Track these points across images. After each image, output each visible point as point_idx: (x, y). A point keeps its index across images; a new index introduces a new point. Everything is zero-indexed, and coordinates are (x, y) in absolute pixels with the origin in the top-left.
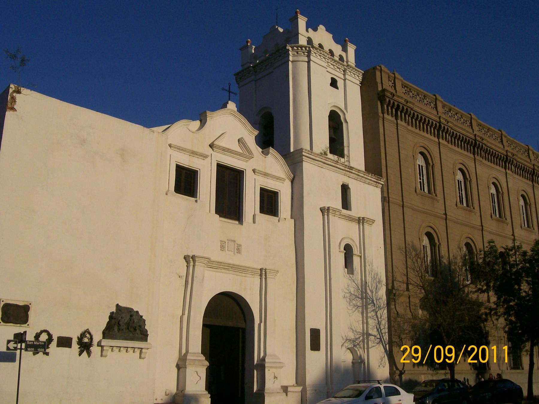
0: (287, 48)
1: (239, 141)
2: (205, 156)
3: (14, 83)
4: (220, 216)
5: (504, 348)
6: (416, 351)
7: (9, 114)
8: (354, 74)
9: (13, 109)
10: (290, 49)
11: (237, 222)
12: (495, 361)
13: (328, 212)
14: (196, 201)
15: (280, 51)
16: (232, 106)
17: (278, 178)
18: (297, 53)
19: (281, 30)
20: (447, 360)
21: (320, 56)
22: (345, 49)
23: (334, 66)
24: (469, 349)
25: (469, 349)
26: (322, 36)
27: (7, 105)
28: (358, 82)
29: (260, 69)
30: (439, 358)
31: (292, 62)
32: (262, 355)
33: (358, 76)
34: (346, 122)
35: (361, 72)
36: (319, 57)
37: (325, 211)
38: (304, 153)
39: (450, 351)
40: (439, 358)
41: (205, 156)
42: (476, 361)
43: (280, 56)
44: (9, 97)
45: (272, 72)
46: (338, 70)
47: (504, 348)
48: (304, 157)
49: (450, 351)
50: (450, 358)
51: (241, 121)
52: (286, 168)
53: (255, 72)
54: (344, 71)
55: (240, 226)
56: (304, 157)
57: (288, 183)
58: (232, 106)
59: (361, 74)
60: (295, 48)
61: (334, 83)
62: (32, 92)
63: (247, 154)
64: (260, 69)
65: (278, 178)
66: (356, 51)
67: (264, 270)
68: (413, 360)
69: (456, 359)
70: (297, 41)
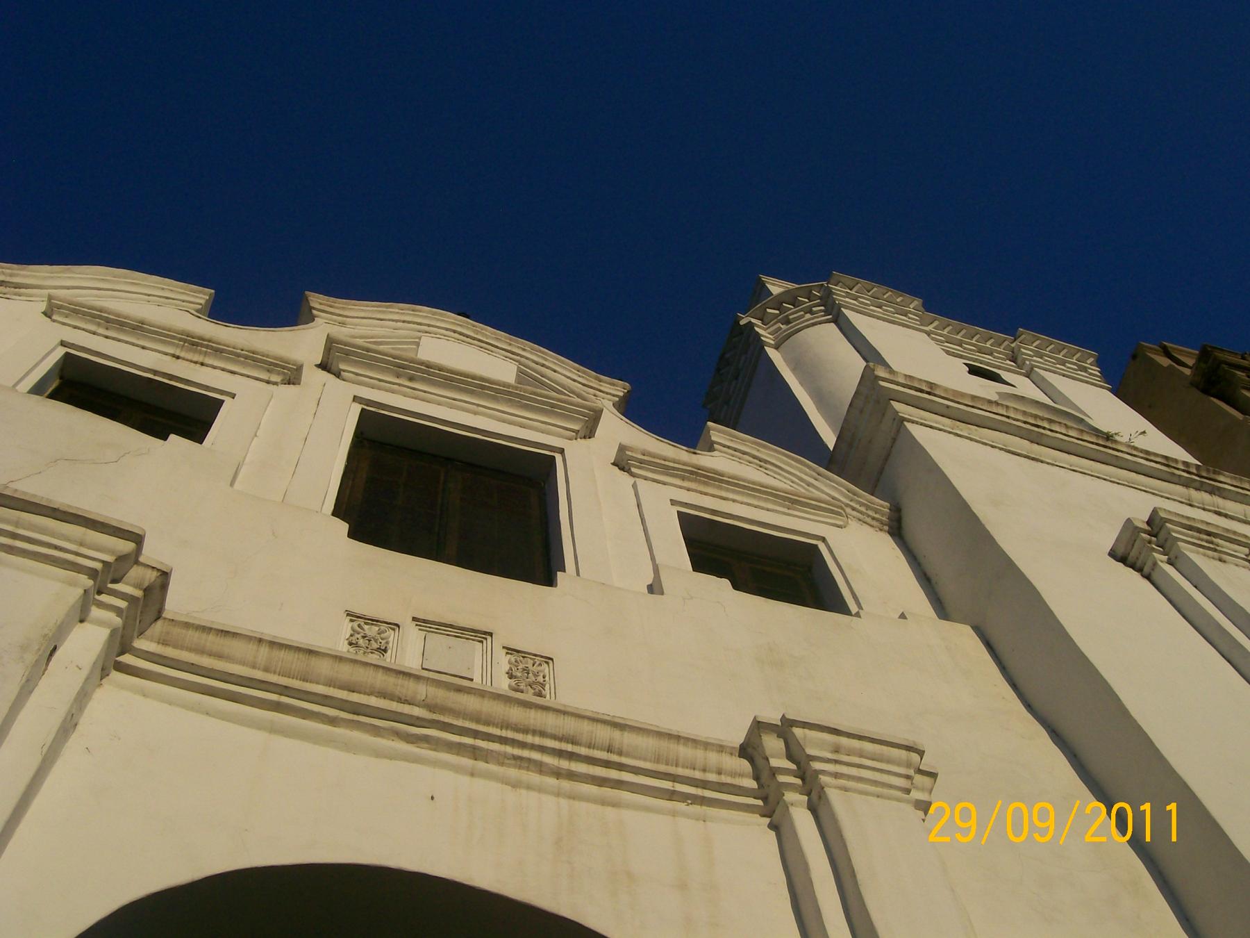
5: (1168, 808)
6: (965, 814)
12: (1174, 839)
13: (1167, 546)
20: (1037, 836)
24: (1088, 811)
25: (1088, 811)
28: (1097, 380)
30: (1018, 832)
31: (777, 347)
32: (633, 470)
37: (1142, 548)
39: (1043, 815)
40: (1018, 832)
42: (1104, 839)
47: (1168, 808)
49: (1043, 815)
50: (1043, 832)
55: (757, 713)
67: (773, 745)
68: (958, 836)
69: (979, 834)
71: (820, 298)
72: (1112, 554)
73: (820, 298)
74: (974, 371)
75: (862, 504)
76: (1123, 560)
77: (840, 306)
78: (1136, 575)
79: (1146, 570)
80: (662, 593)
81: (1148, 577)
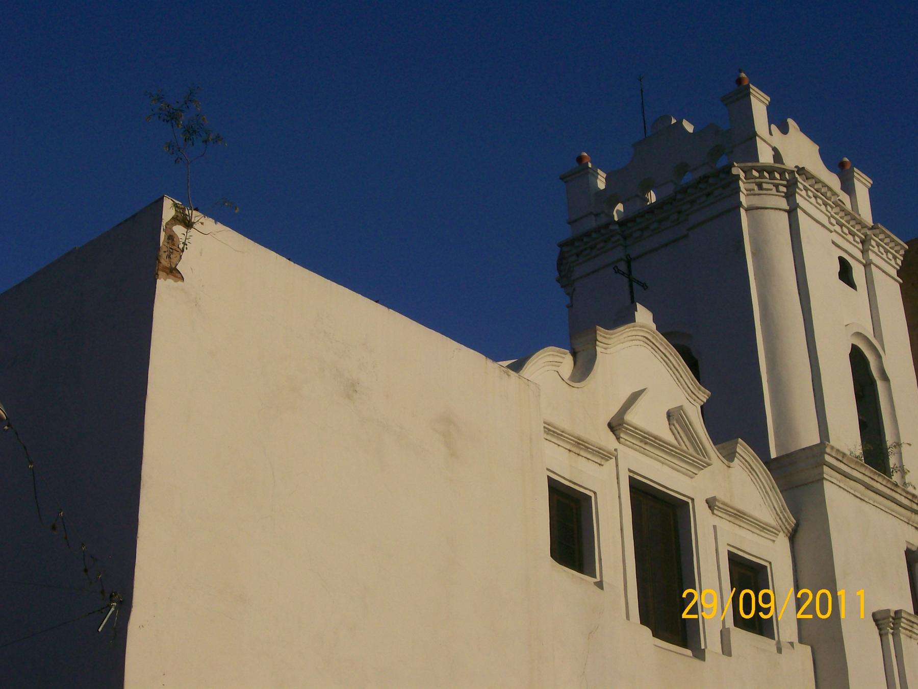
0: (735, 171)
1: (669, 415)
2: (604, 455)
3: (173, 195)
4: (655, 635)
7: (164, 285)
8: (887, 252)
9: (174, 272)
10: (742, 175)
11: (689, 652)
13: (896, 627)
14: (600, 585)
15: (711, 181)
16: (643, 315)
17: (763, 527)
18: (760, 186)
19: (689, 127)
20: (761, 614)
21: (816, 197)
22: (848, 187)
23: (841, 225)
26: (798, 149)
27: (157, 259)
28: (894, 273)
29: (642, 230)
31: (747, 210)
33: (895, 258)
34: (885, 378)
35: (903, 248)
36: (813, 200)
37: (885, 622)
38: (828, 458)
41: (604, 455)
43: (708, 195)
44: (163, 234)
45: (686, 236)
46: (850, 238)
48: (825, 468)
51: (667, 362)
52: (777, 499)
53: (625, 238)
54: (863, 242)
56: (825, 468)
57: (783, 542)
58: (643, 315)
59: (902, 252)
60: (755, 174)
61: (845, 273)
62: (220, 226)
63: (691, 451)
64: (642, 230)
65: (763, 527)
66: (872, 191)
70: (755, 157)
71: (787, 181)
72: (874, 615)
73: (787, 181)
74: (857, 359)
75: (784, 517)
76: (876, 620)
77: (797, 206)
78: (877, 631)
79: (883, 632)
80: (730, 655)
81: (881, 635)
